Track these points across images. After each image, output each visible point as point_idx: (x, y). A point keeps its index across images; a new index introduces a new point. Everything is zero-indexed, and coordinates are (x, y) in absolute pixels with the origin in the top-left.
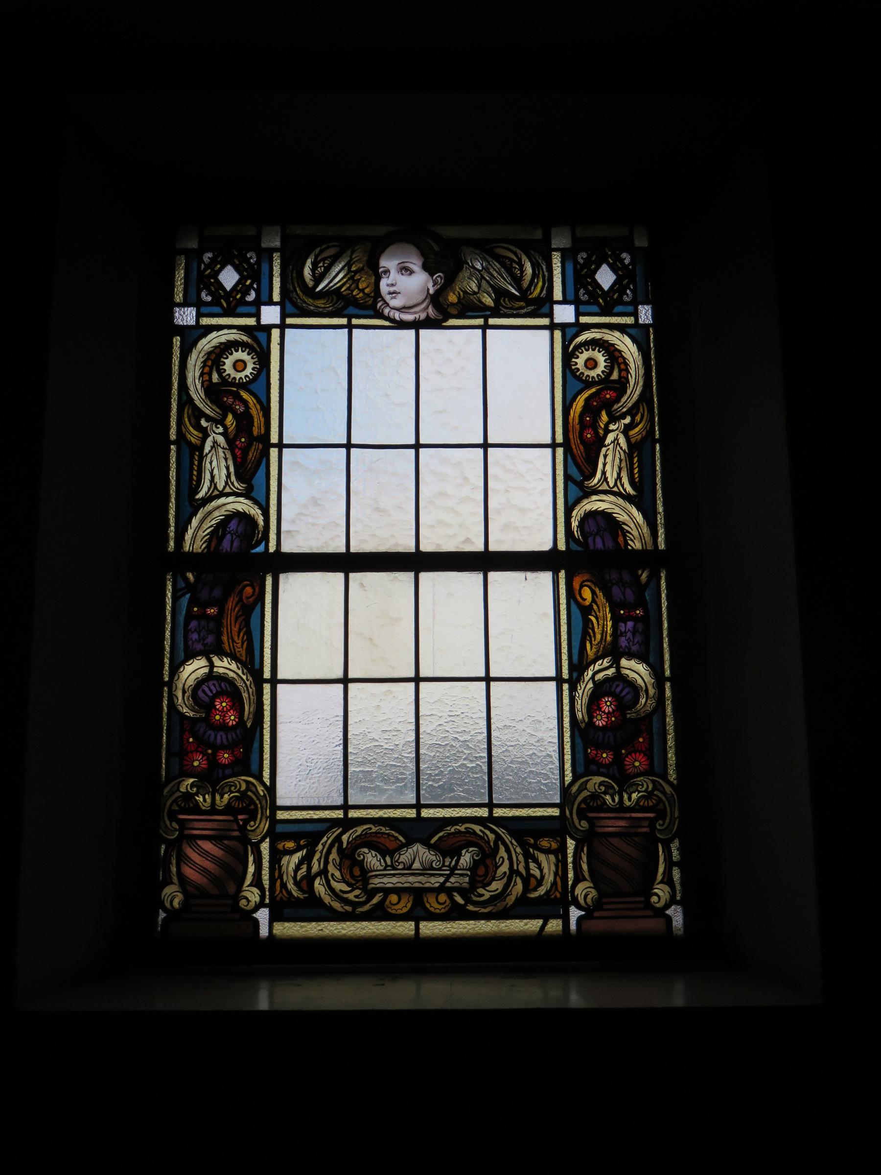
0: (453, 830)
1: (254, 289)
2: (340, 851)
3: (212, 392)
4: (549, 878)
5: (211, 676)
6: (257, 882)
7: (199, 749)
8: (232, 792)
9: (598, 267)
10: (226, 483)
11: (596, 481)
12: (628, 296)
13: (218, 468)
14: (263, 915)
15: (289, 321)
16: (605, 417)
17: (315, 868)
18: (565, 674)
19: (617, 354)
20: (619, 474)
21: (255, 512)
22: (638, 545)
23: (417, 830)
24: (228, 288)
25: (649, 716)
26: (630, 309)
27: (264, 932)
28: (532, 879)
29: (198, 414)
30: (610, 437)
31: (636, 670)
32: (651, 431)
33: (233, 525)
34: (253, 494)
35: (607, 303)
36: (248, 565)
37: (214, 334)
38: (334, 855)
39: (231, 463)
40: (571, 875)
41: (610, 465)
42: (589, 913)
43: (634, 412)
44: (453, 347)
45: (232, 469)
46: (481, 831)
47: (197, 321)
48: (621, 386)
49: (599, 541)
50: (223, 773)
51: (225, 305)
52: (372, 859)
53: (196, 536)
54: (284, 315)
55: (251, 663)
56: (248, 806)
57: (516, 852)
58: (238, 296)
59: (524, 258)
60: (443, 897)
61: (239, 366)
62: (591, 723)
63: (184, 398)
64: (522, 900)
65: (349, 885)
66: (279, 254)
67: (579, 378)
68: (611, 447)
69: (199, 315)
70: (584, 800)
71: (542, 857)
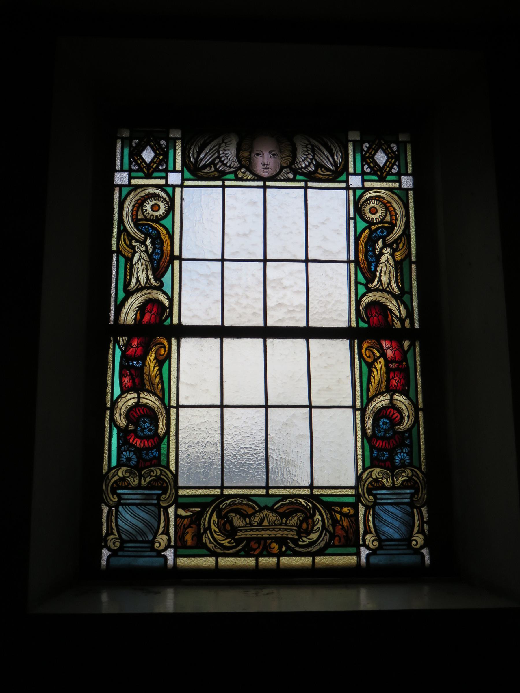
3: (137, 223)
5: (138, 405)
6: (166, 532)
8: (151, 476)
9: (376, 152)
11: (375, 283)
14: (170, 554)
16: (380, 244)
18: (358, 406)
24: (148, 162)
25: (409, 430)
27: (170, 561)
30: (383, 259)
32: (409, 255)
34: (163, 289)
35: (381, 174)
36: (161, 328)
41: (386, 274)
42: (374, 552)
43: (399, 242)
44: (286, 200)
47: (129, 181)
51: (146, 171)
52: (238, 521)
53: (129, 314)
54: (183, 179)
56: (162, 484)
63: (122, 228)
68: (384, 265)
69: (130, 178)
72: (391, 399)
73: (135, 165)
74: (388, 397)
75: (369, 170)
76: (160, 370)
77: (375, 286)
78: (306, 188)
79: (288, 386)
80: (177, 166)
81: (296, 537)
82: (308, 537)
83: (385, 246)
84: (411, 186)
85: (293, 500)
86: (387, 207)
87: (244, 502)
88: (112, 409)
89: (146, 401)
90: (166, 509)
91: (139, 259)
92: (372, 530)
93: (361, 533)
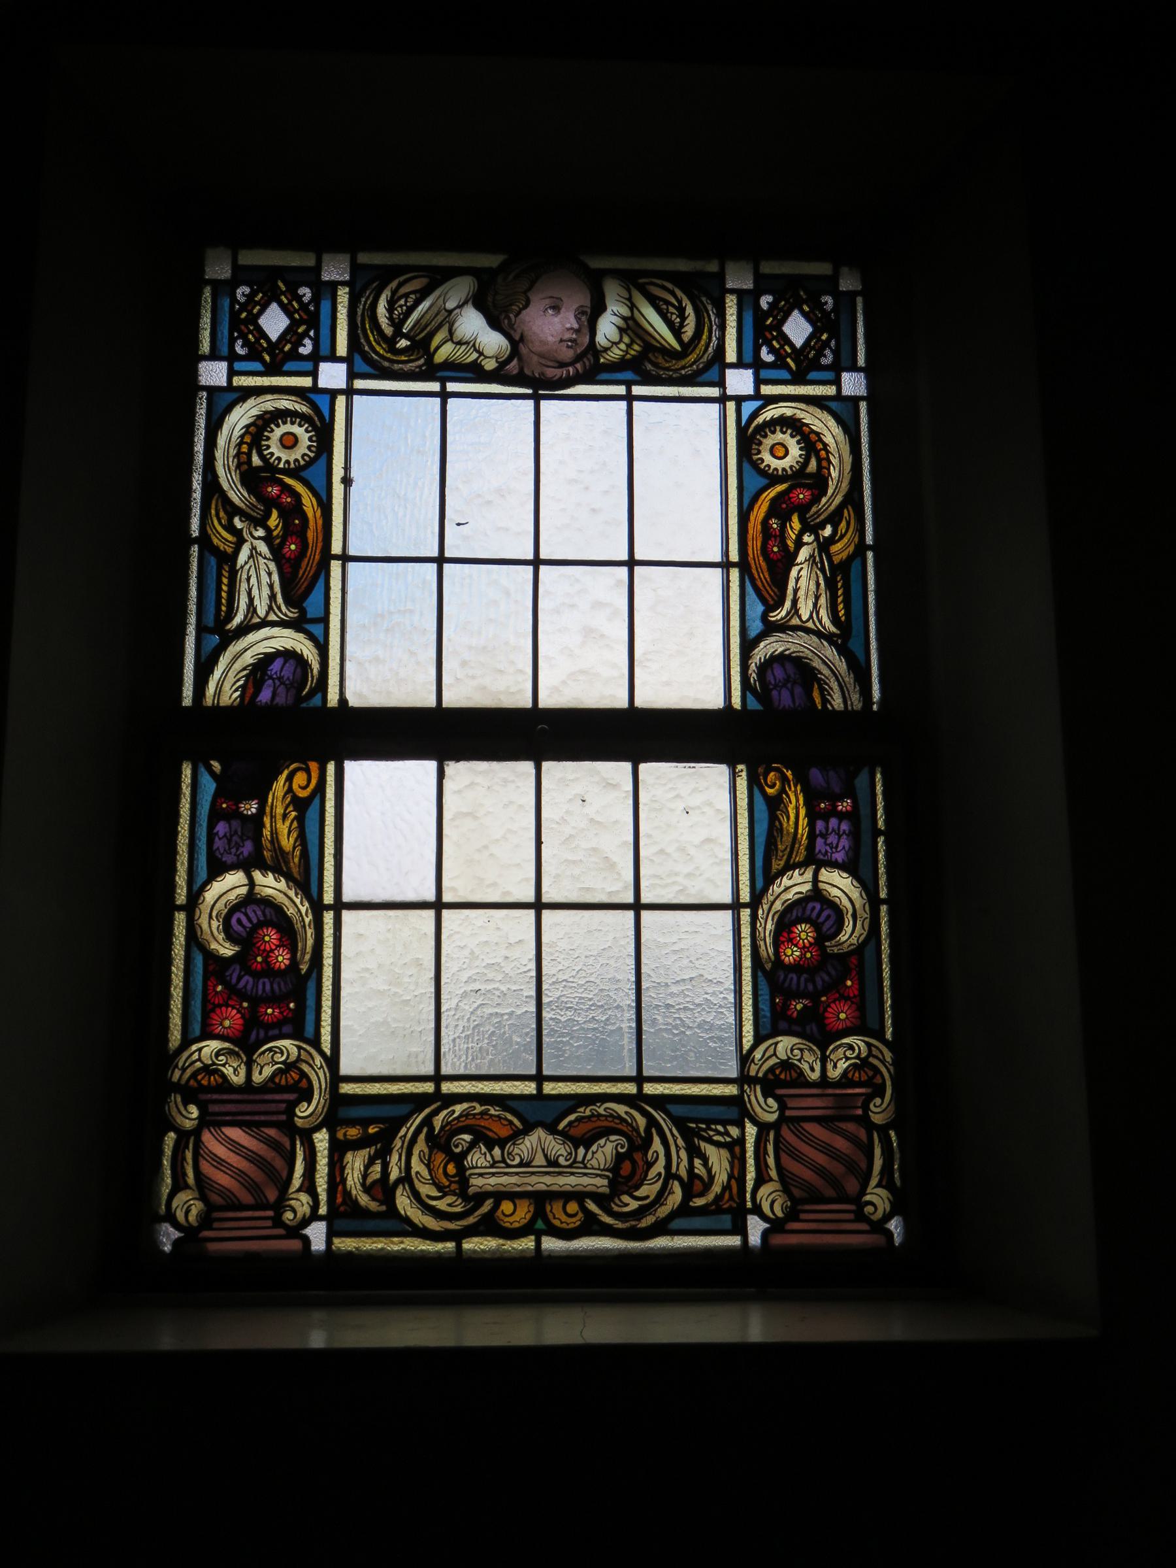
0: (588, 1113)
1: (310, 338)
2: (431, 1139)
3: (251, 478)
4: (721, 1178)
5: (251, 898)
6: (309, 1186)
7: (230, 1002)
10: (270, 608)
12: (828, 359)
13: (258, 581)
14: (317, 1233)
15: (359, 384)
17: (394, 1174)
19: (813, 437)
20: (815, 605)
21: (308, 650)
22: (837, 703)
23: (540, 1110)
25: (860, 949)
26: (829, 375)
28: (697, 1182)
29: (233, 510)
30: (804, 554)
31: (839, 885)
33: (276, 666)
35: (803, 365)
37: (251, 402)
38: (421, 1145)
39: (275, 577)
40: (751, 1175)
42: (775, 1226)
44: (583, 424)
45: (277, 588)
46: (626, 1113)
48: (819, 483)
49: (785, 694)
50: (266, 1033)
53: (225, 684)
54: (352, 375)
55: (306, 880)
57: (678, 1157)
58: (287, 348)
59: (687, 303)
60: (573, 1207)
61: (288, 446)
62: (778, 962)
63: (210, 477)
64: (684, 1210)
65: (439, 1188)
66: (347, 290)
67: (763, 473)
69: (232, 373)
70: (771, 1070)
71: (710, 1151)
72: (815, 880)
73: (243, 294)
74: (809, 875)
75: (769, 358)
76: (300, 819)
77: (782, 619)
78: (630, 398)
79: (587, 862)
80: (338, 348)
81: (607, 1190)
82: (637, 1194)
83: (806, 528)
84: (862, 391)
85: (601, 1111)
86: (811, 443)
87: (492, 1112)
88: (192, 906)
89: (270, 891)
90: (307, 1136)
91: (251, 556)
92: (773, 1173)
93: (750, 1185)
